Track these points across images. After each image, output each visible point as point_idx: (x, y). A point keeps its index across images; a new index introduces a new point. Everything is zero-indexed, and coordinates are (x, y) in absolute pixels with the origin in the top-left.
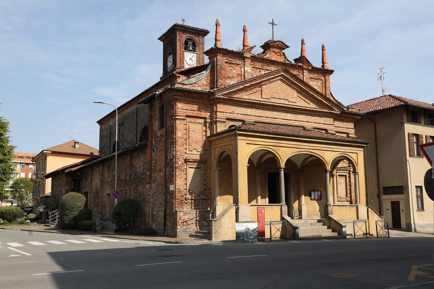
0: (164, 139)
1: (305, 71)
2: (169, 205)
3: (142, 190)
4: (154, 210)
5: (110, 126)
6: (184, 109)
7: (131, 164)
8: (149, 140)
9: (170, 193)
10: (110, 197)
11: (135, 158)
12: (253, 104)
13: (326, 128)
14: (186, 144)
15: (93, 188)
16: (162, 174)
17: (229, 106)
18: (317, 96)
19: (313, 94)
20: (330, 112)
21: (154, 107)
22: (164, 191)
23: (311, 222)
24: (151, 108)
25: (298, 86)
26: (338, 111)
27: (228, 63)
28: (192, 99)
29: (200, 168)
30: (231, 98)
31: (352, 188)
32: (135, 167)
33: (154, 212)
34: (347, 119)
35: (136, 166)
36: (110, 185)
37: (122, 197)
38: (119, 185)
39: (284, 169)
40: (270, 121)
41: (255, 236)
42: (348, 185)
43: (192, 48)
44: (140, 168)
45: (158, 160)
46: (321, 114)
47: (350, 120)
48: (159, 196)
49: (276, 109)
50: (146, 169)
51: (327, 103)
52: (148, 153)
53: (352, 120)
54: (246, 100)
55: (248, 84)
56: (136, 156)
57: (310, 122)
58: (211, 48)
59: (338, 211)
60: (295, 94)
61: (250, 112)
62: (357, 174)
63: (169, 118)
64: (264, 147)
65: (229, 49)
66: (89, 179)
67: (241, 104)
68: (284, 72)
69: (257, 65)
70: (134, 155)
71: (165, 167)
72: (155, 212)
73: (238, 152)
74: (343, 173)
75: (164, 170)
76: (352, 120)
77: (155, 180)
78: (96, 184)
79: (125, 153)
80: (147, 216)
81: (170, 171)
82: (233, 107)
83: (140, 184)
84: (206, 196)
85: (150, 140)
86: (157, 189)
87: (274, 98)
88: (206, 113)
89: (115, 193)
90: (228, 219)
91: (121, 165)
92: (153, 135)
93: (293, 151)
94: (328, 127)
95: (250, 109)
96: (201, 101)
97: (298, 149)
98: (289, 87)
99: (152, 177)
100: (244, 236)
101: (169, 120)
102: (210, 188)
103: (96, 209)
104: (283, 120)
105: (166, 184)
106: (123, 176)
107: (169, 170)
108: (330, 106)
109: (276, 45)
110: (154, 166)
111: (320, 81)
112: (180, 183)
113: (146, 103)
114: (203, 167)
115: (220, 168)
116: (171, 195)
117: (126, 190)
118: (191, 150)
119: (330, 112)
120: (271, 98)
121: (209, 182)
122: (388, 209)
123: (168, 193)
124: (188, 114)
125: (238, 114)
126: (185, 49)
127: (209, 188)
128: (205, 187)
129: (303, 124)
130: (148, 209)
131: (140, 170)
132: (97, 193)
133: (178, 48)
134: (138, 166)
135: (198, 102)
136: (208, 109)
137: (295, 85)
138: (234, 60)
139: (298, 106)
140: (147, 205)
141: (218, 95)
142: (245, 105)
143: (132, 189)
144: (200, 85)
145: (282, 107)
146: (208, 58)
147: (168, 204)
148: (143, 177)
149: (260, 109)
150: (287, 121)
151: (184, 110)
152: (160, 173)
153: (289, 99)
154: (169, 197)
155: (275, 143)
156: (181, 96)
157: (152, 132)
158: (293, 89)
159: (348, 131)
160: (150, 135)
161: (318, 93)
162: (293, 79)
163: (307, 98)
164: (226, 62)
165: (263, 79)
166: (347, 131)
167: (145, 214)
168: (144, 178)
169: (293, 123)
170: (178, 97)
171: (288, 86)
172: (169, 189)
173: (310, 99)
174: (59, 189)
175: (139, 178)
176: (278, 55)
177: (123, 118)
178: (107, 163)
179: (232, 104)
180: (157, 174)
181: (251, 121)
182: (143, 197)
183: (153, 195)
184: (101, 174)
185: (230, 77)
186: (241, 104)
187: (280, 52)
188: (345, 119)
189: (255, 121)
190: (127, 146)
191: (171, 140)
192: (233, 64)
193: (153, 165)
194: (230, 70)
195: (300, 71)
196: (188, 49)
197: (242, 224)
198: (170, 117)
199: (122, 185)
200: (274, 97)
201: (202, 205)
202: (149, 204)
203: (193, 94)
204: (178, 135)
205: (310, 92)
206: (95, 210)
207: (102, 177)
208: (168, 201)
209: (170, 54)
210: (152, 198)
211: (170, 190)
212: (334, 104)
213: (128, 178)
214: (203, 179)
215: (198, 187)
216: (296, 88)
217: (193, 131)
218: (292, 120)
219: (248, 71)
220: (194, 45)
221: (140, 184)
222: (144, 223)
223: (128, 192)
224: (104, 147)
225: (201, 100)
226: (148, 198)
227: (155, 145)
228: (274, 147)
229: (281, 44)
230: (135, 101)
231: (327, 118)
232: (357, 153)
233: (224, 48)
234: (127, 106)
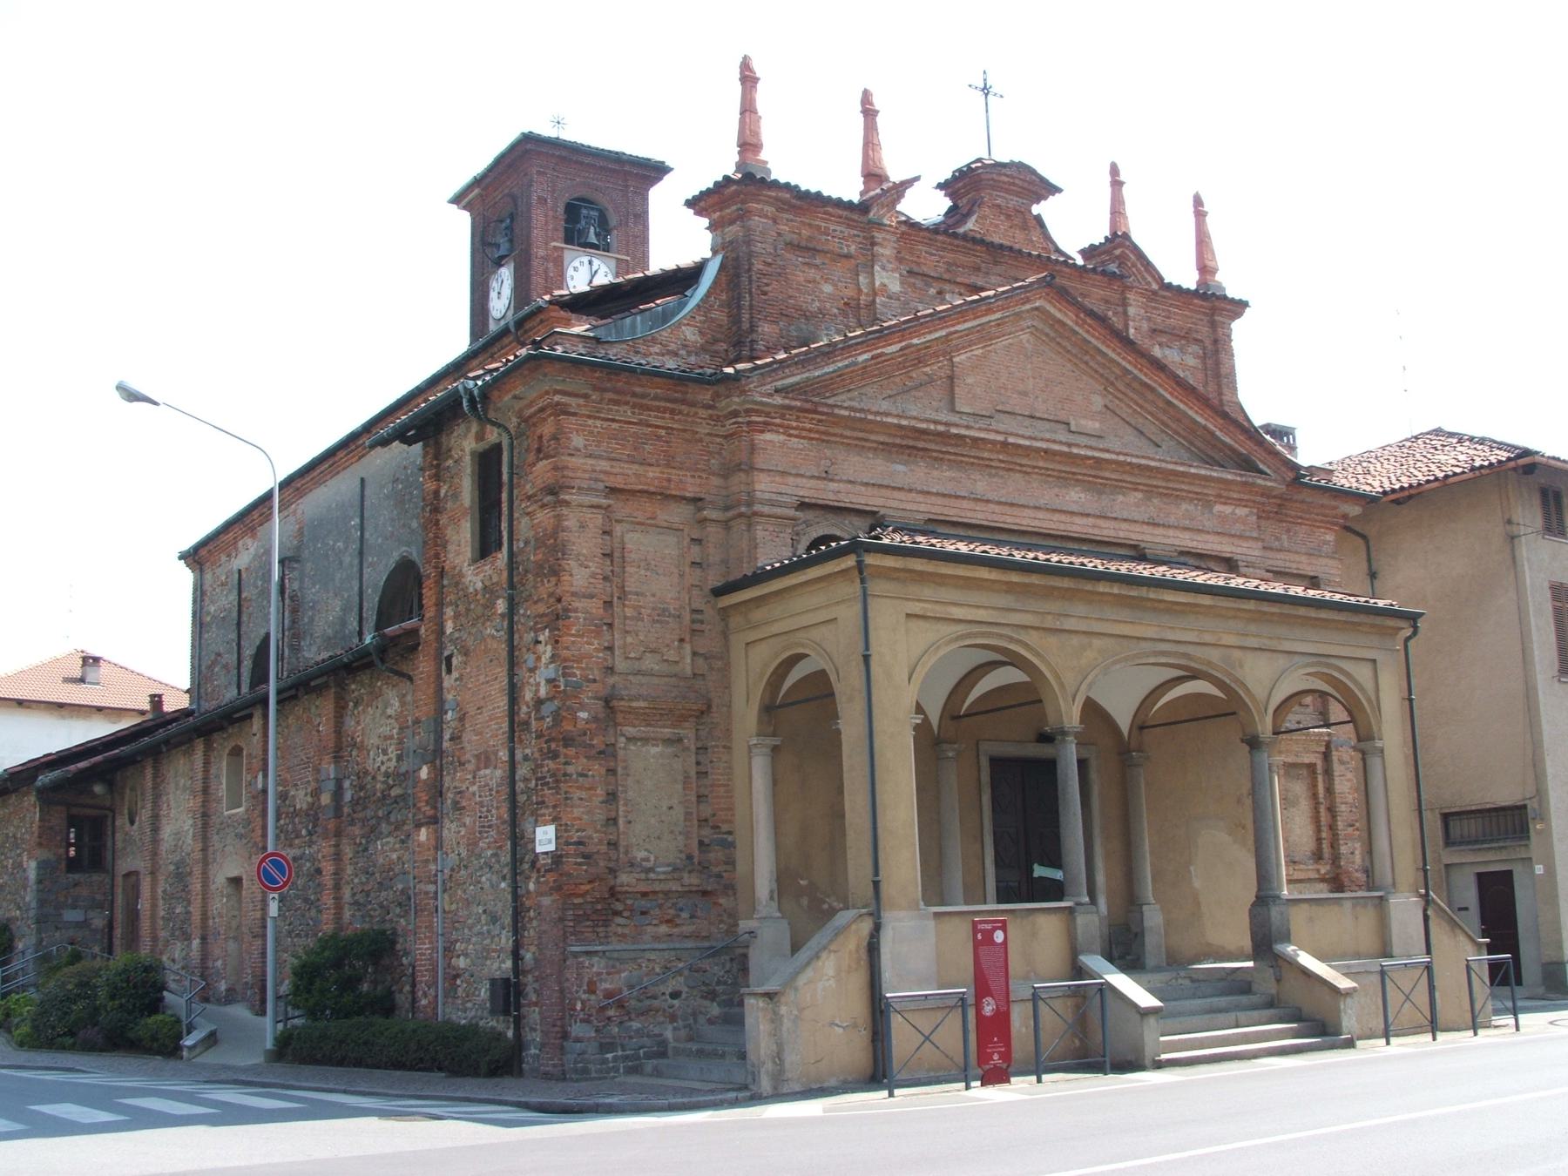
0: (501, 606)
2: (535, 923)
3: (394, 856)
4: (457, 948)
5: (240, 571)
7: (340, 733)
8: (427, 615)
9: (538, 865)
10: (244, 892)
11: (356, 704)
14: (610, 625)
15: (164, 853)
16: (495, 775)
21: (451, 457)
22: (506, 858)
24: (435, 462)
28: (636, 411)
29: (680, 740)
31: (1339, 818)
32: (361, 747)
33: (458, 956)
35: (362, 742)
36: (241, 836)
37: (298, 890)
38: (282, 835)
39: (1077, 735)
42: (1322, 809)
43: (597, 235)
44: (385, 752)
45: (472, 711)
47: (1322, 521)
48: (479, 882)
49: (1021, 465)
50: (411, 753)
52: (421, 679)
56: (365, 698)
57: (1164, 525)
58: (720, 179)
61: (905, 474)
63: (523, 506)
64: (983, 635)
65: (803, 188)
66: (145, 815)
67: (861, 435)
70: (353, 692)
71: (511, 739)
72: (462, 958)
73: (870, 655)
75: (503, 755)
77: (457, 806)
78: (177, 834)
79: (312, 684)
80: (424, 978)
81: (535, 760)
83: (384, 825)
84: (710, 876)
85: (430, 613)
86: (472, 844)
89: (267, 865)
91: (289, 743)
92: (445, 590)
96: (680, 420)
99: (444, 791)
101: (528, 514)
102: (730, 838)
103: (177, 950)
105: (514, 822)
106: (301, 793)
107: (528, 751)
110: (451, 739)
111: (1195, 348)
113: (409, 442)
114: (692, 735)
115: (777, 741)
116: (544, 876)
117: (320, 857)
118: (632, 655)
120: (997, 416)
121: (722, 809)
122: (1466, 909)
123: (526, 866)
124: (618, 482)
126: (569, 240)
127: (725, 836)
128: (706, 832)
129: (1133, 536)
130: (429, 943)
131: (383, 763)
132: (180, 876)
133: (537, 234)
134: (373, 740)
135: (663, 428)
136: (713, 461)
139: (1114, 452)
140: (421, 927)
143: (348, 851)
144: (673, 347)
146: (707, 228)
147: (527, 919)
148: (395, 792)
152: (482, 772)
153: (1073, 423)
154: (532, 886)
157: (442, 577)
160: (431, 589)
167: (414, 967)
168: (403, 797)
170: (573, 401)
172: (530, 847)
174: (11, 861)
175: (379, 800)
177: (300, 529)
178: (225, 736)
180: (469, 776)
182: (400, 887)
183: (451, 876)
184: (199, 785)
185: (808, 314)
186: (861, 435)
189: (929, 520)
190: (314, 654)
191: (536, 607)
193: (447, 736)
196: (578, 239)
198: (529, 498)
199: (297, 837)
201: (691, 918)
202: (431, 922)
204: (575, 583)
206: (176, 956)
207: (203, 802)
208: (528, 903)
209: (499, 263)
210: (445, 891)
211: (538, 851)
213: (326, 799)
214: (694, 792)
215: (672, 832)
217: (642, 564)
219: (891, 286)
220: (604, 226)
221: (384, 825)
222: (407, 1011)
223: (328, 868)
224: (210, 667)
225: (676, 417)
226: (427, 893)
227: (457, 639)
230: (353, 451)
232: (1374, 661)
233: (782, 180)
234: (315, 474)
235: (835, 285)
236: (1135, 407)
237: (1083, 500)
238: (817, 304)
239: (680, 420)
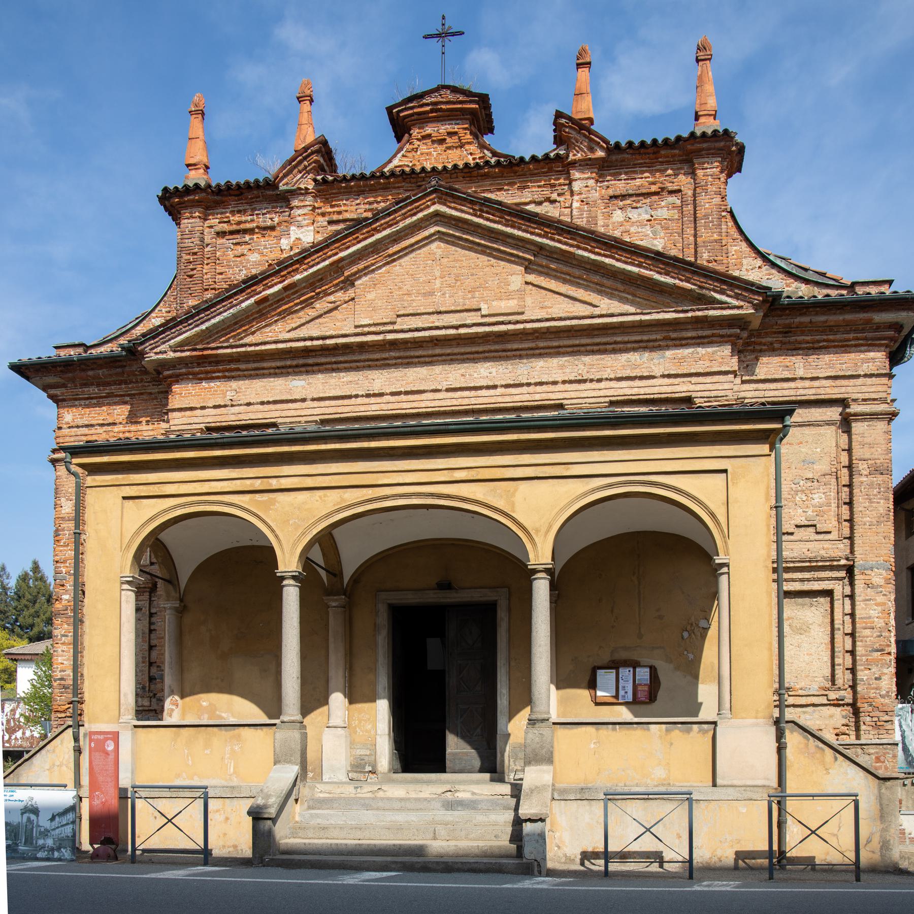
1: (576, 174)
6: (78, 427)
12: (308, 357)
13: (688, 394)
17: (218, 383)
18: (618, 260)
19: (593, 257)
20: (697, 318)
23: (473, 793)
25: (520, 244)
26: (742, 303)
27: (232, 233)
30: (206, 353)
34: (831, 337)
40: (390, 406)
41: (62, 840)
46: (653, 337)
51: (677, 282)
53: (866, 339)
54: (263, 347)
55: (276, 284)
59: (592, 746)
60: (516, 276)
61: (303, 387)
62: (723, 574)
68: (440, 203)
69: (346, 211)
74: (808, 580)
76: (866, 339)
82: (234, 384)
87: (408, 315)
88: (156, 426)
90: (47, 772)
93: (343, 500)
94: (698, 387)
95: (304, 377)
96: (133, 387)
97: (365, 490)
98: (486, 258)
100: (15, 836)
104: (450, 395)
108: (691, 290)
109: (428, 108)
111: (675, 200)
112: (65, 662)
119: (697, 320)
120: (399, 320)
125: (249, 404)
137: (505, 244)
138: (249, 218)
141: (155, 350)
142: (278, 368)
145: (436, 345)
149: (345, 368)
150: (473, 393)
151: (81, 429)
155: (248, 482)
156: (64, 386)
158: (502, 263)
159: (843, 390)
161: (616, 247)
162: (488, 219)
163: (579, 284)
164: (221, 234)
165: (341, 250)
166: (836, 390)
169: (500, 399)
171: (479, 256)
173: (591, 285)
176: (449, 148)
179: (227, 374)
181: (300, 422)
187: (456, 130)
188: (818, 337)
192: (251, 231)
194: (235, 256)
195: (558, 179)
197: (12, 794)
200: (411, 312)
203: (92, 369)
205: (580, 252)
212: (711, 278)
216: (515, 252)
218: (495, 387)
225: (130, 386)
228: (247, 497)
229: (451, 97)
231: (691, 350)
232: (725, 471)
235: (262, 254)
236: (564, 276)
237: (494, 374)
238: (244, 272)
239: (133, 387)
